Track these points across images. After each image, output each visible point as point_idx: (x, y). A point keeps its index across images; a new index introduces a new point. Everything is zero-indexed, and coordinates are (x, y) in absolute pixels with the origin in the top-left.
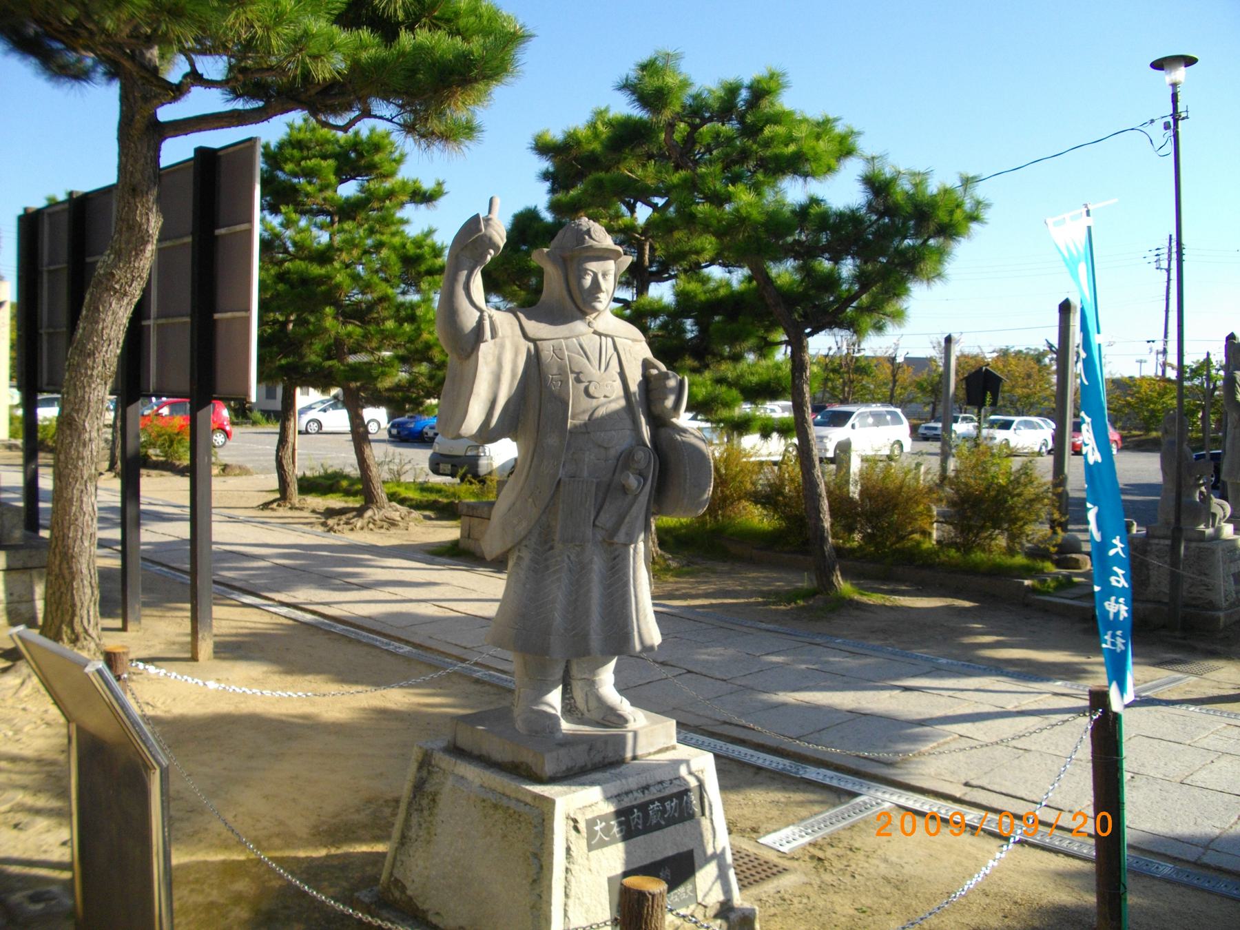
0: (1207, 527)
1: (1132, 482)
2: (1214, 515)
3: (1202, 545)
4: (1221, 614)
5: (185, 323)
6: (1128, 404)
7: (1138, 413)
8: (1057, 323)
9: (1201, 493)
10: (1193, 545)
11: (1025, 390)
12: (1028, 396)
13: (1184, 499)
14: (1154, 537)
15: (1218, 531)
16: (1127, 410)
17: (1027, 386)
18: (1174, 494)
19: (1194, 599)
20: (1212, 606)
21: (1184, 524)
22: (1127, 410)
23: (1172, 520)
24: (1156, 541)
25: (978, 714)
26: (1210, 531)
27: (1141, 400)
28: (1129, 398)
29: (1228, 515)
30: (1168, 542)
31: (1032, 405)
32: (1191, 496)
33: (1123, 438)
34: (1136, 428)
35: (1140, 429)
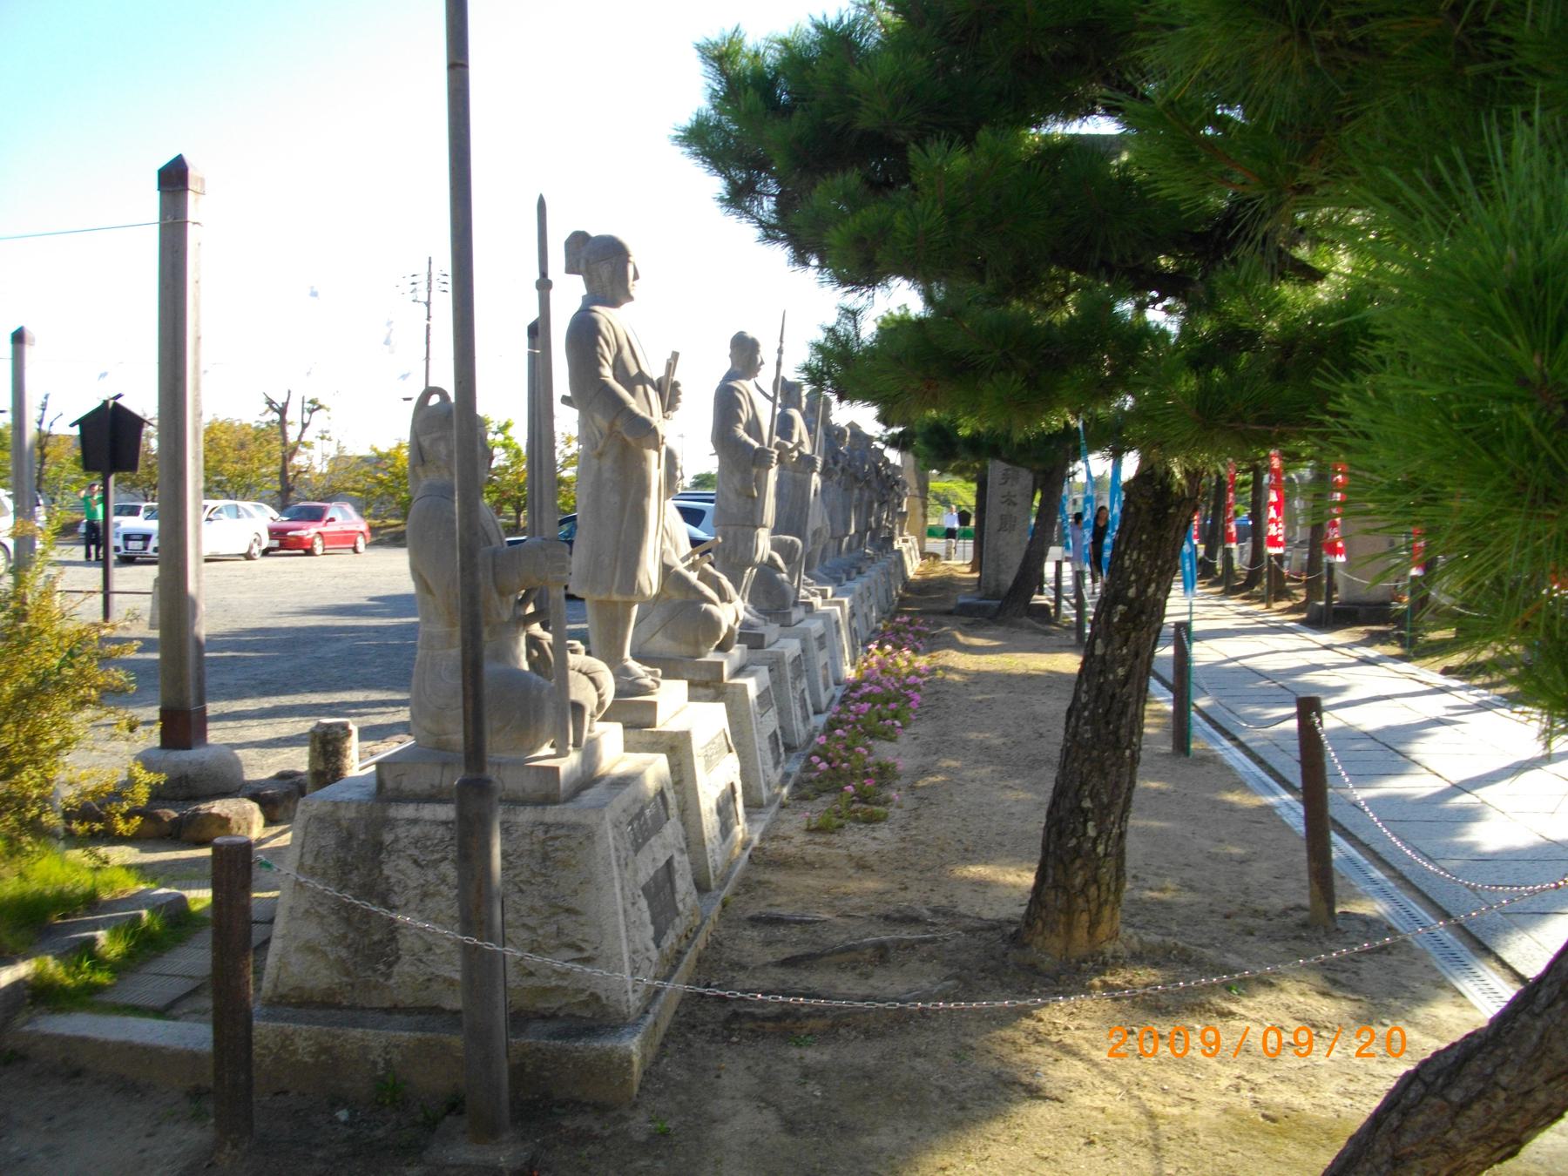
0: (562, 753)
1: (383, 593)
2: (578, 708)
3: (551, 814)
4: (633, 1045)
5: (1052, 680)
6: (381, 483)
7: (393, 495)
8: (155, 215)
9: (533, 642)
10: (526, 816)
11: (238, 466)
12: (242, 475)
13: (490, 668)
14: (402, 798)
15: (590, 753)
16: (379, 491)
17: (241, 459)
18: (456, 652)
19: (545, 992)
20: (597, 1018)
21: (496, 746)
22: (379, 491)
23: (457, 737)
24: (408, 811)
25: (277, 746)
26: (568, 764)
27: (396, 475)
28: (380, 475)
29: (609, 698)
30: (447, 812)
31: (249, 487)
32: (505, 653)
33: (372, 529)
34: (391, 516)
35: (397, 517)
